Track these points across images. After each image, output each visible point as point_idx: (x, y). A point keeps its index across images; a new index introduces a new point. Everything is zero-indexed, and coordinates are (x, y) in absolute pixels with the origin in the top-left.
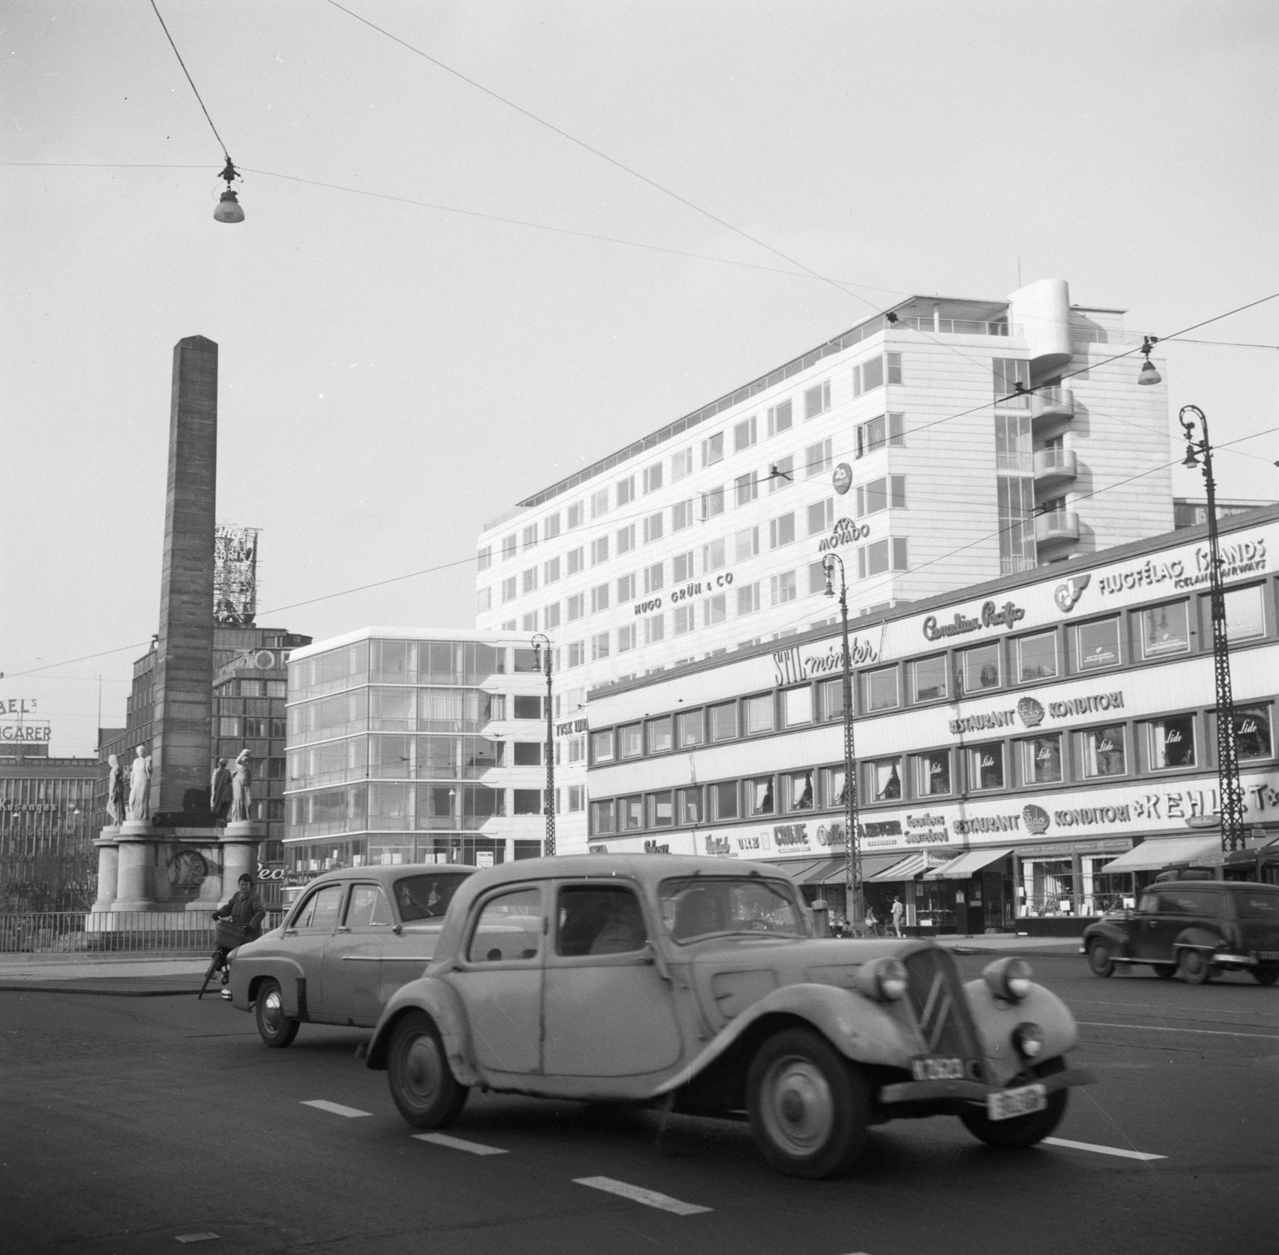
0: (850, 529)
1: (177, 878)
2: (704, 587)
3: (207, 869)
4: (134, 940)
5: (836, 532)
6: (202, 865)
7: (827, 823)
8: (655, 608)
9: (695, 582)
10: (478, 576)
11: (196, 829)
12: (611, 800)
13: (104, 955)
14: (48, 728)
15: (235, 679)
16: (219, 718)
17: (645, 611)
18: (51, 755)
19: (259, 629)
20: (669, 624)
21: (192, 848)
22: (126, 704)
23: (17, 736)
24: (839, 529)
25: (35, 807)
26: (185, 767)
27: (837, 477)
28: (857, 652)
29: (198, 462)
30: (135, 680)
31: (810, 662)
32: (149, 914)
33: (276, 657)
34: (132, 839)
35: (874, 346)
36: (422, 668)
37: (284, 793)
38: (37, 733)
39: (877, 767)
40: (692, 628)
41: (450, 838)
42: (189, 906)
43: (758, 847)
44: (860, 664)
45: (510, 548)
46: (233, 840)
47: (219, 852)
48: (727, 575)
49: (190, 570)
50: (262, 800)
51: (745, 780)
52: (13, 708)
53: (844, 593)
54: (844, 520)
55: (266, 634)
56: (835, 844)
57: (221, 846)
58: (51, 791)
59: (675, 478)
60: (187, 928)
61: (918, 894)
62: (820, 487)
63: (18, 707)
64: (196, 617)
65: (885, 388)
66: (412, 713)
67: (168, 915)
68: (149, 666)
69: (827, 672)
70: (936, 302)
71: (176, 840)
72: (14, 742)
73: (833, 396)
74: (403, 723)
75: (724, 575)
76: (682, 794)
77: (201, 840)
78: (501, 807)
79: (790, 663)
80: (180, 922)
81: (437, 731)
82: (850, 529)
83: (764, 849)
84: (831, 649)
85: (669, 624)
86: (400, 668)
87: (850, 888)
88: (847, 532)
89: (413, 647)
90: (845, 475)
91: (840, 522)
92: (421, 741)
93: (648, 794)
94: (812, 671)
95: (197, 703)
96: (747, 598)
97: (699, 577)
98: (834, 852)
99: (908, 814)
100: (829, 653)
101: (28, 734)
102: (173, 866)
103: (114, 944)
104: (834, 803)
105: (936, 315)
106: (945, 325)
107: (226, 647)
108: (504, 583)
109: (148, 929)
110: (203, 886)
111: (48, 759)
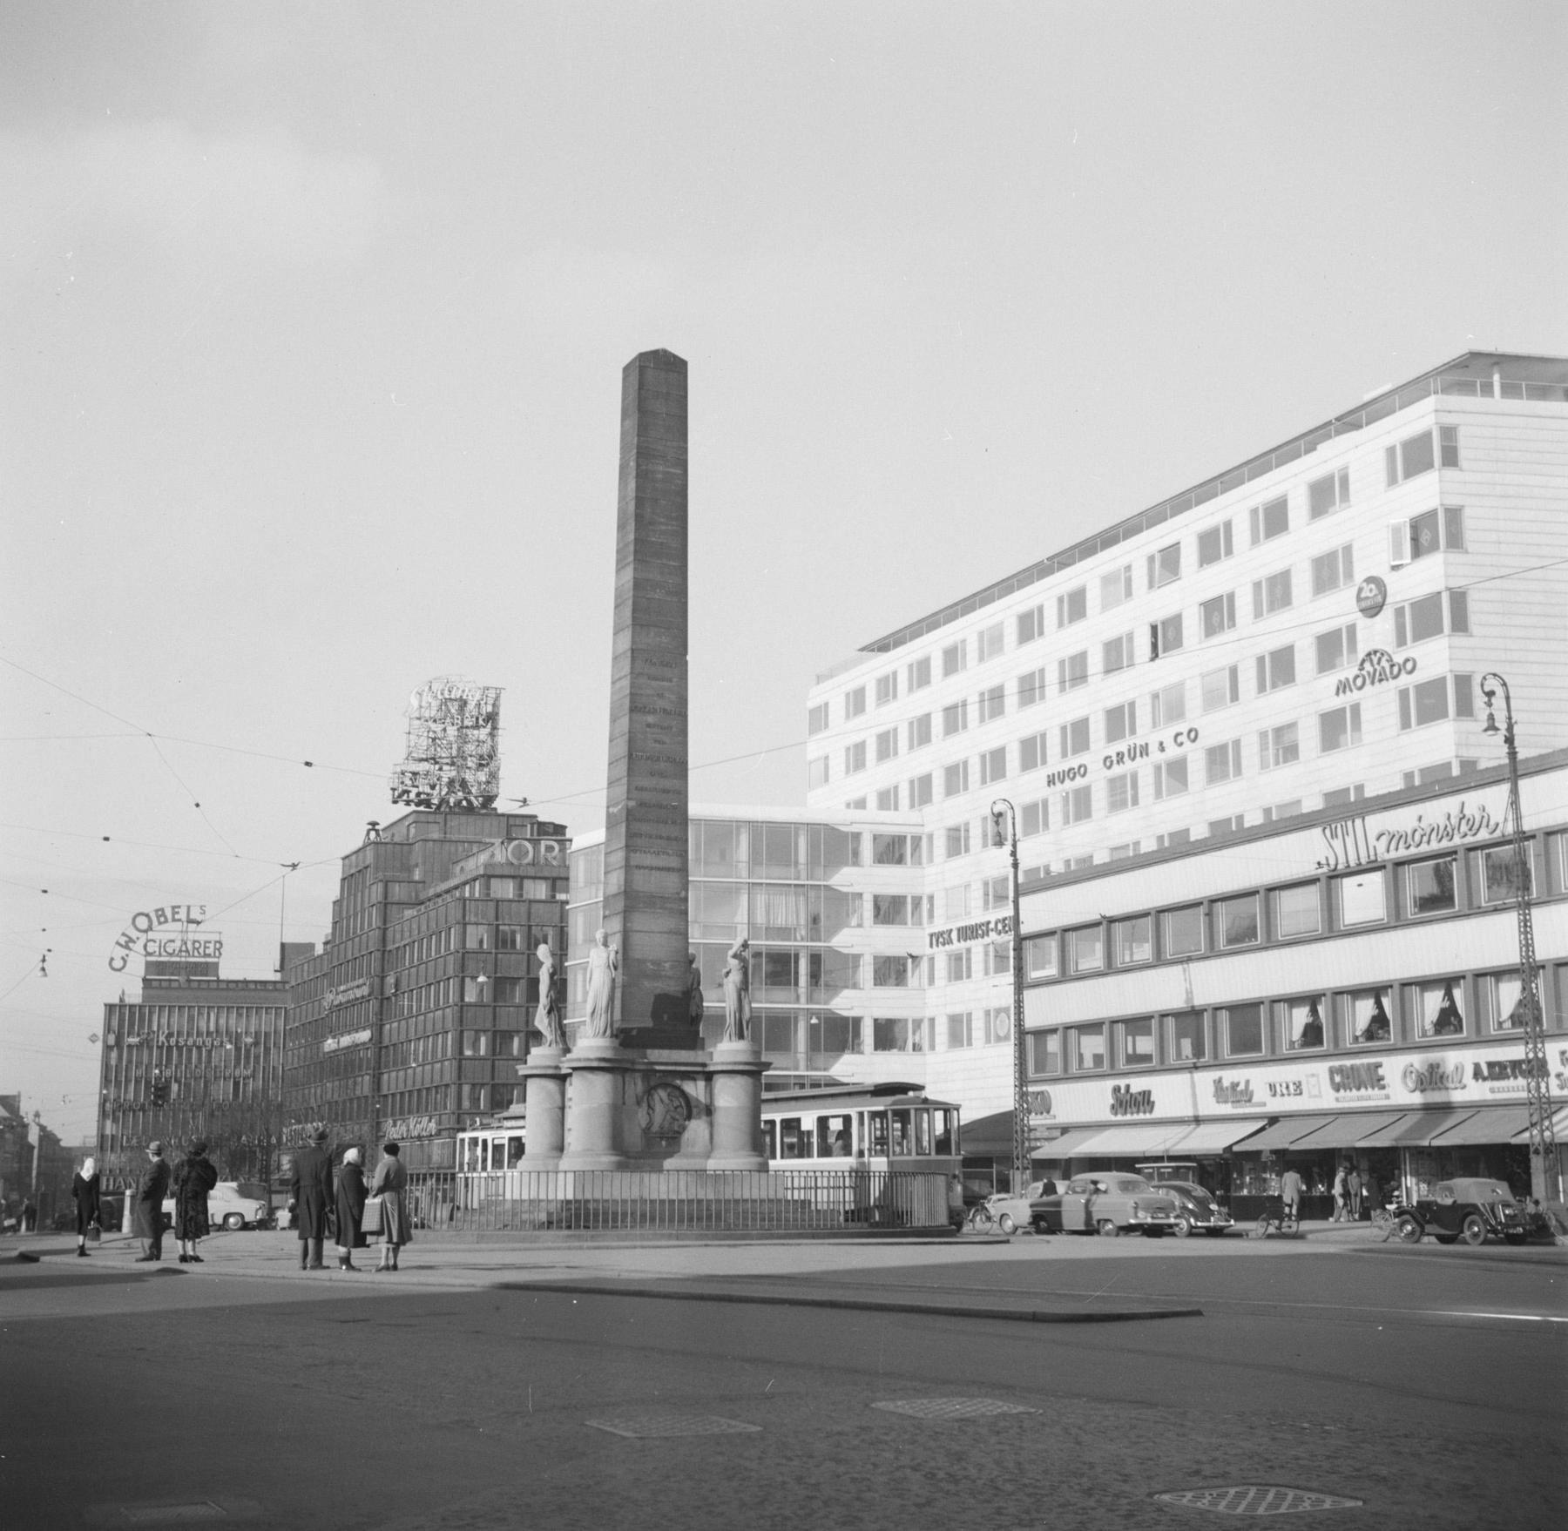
0: (1384, 663)
1: (650, 1124)
2: (1153, 748)
3: (690, 1109)
4: (605, 1213)
5: (1361, 669)
6: (683, 1104)
7: (1417, 1060)
8: (1078, 778)
9: (1140, 742)
11: (674, 1052)
12: (1054, 1031)
13: (592, 1237)
14: (220, 942)
15: (483, 876)
16: (465, 925)
17: (1062, 782)
18: (223, 976)
19: (503, 815)
20: (1099, 798)
21: (669, 1080)
22: (331, 910)
23: (180, 951)
24: (1367, 666)
25: (204, 1042)
26: (653, 963)
27: (1363, 595)
28: (1464, 822)
29: (663, 528)
30: (343, 879)
31: (1384, 838)
32: (618, 1175)
33: (534, 848)
34: (595, 1064)
35: (1420, 417)
36: (755, 859)
37: (565, 1022)
38: (205, 947)
39: (1497, 982)
40: (1135, 802)
42: (668, 1164)
43: (1301, 1094)
44: (1469, 840)
45: (856, 703)
46: (730, 1068)
47: (706, 1086)
48: (1190, 731)
49: (656, 679)
50: (518, 1032)
51: (1275, 1001)
52: (177, 917)
53: (1510, 728)
54: (1375, 652)
55: (512, 821)
56: (1433, 1089)
57: (709, 1077)
58: (222, 1021)
59: (1105, 607)
60: (673, 1197)
62: (1339, 608)
63: (182, 915)
64: (665, 746)
65: (1437, 472)
66: (742, 917)
67: (646, 1176)
68: (364, 862)
69: (1413, 850)
70: (1495, 359)
71: (649, 1067)
72: (178, 959)
73: (1352, 487)
74: (731, 930)
75: (1185, 732)
76: (1170, 1023)
78: (856, 1042)
79: (1350, 840)
80: (663, 1188)
82: (1384, 663)
83: (1310, 1097)
84: (1420, 819)
85: (1099, 798)
86: (723, 855)
87: (1537, 1152)
88: (1378, 668)
89: (743, 830)
90: (1375, 591)
91: (1369, 654)
93: (1114, 1022)
94: (1388, 851)
95: (668, 869)
96: (1222, 761)
97: (1145, 732)
99: (1563, 1049)
100: (1415, 824)
101: (194, 948)
102: (645, 1105)
103: (587, 1220)
104: (1424, 1035)
105: (1496, 378)
106: (1510, 390)
107: (462, 837)
108: (848, 749)
109: (626, 1196)
110: (686, 1136)
111: (218, 981)
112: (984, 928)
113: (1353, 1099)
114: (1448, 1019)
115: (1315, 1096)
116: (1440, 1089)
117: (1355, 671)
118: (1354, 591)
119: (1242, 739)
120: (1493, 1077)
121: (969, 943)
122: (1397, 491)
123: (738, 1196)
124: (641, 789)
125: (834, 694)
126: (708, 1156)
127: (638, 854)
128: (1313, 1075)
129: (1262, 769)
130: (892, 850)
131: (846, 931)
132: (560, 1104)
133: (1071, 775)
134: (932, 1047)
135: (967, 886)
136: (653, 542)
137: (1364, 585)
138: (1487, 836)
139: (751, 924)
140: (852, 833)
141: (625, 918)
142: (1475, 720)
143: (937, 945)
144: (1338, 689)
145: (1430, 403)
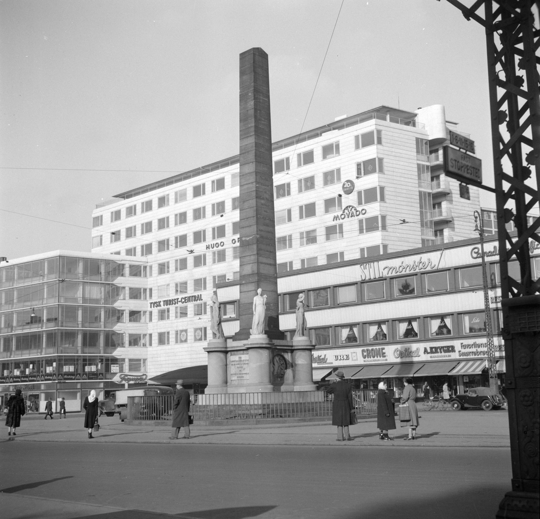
0: (353, 210)
10: (92, 230)
24: (346, 211)
27: (345, 186)
29: (263, 122)
31: (391, 269)
34: (264, 346)
35: (370, 126)
41: (76, 358)
44: (422, 270)
45: (117, 215)
46: (302, 348)
54: (350, 206)
61: (465, 381)
62: (335, 190)
66: (80, 294)
69: (398, 274)
70: (388, 110)
77: (285, 348)
80: (289, 398)
81: (92, 304)
82: (353, 210)
84: (402, 263)
91: (347, 207)
92: (85, 309)
98: (402, 361)
100: (400, 264)
112: (176, 301)
113: (371, 361)
114: (410, 333)
115: (355, 360)
116: (409, 357)
117: (341, 213)
118: (342, 184)
119: (293, 235)
120: (432, 352)
121: (168, 306)
122: (359, 151)
123: (313, 400)
124: (261, 231)
125: (106, 212)
126: (293, 385)
127: (261, 258)
128: (354, 353)
129: (301, 245)
130: (136, 271)
131: (119, 301)
132: (226, 364)
133: (217, 246)
134: (151, 344)
135: (168, 285)
136: (260, 128)
137: (346, 183)
138: (430, 269)
139: (84, 298)
140: (122, 264)
141: (258, 284)
142: (387, 232)
143: (154, 307)
144: (334, 218)
145: (373, 121)
